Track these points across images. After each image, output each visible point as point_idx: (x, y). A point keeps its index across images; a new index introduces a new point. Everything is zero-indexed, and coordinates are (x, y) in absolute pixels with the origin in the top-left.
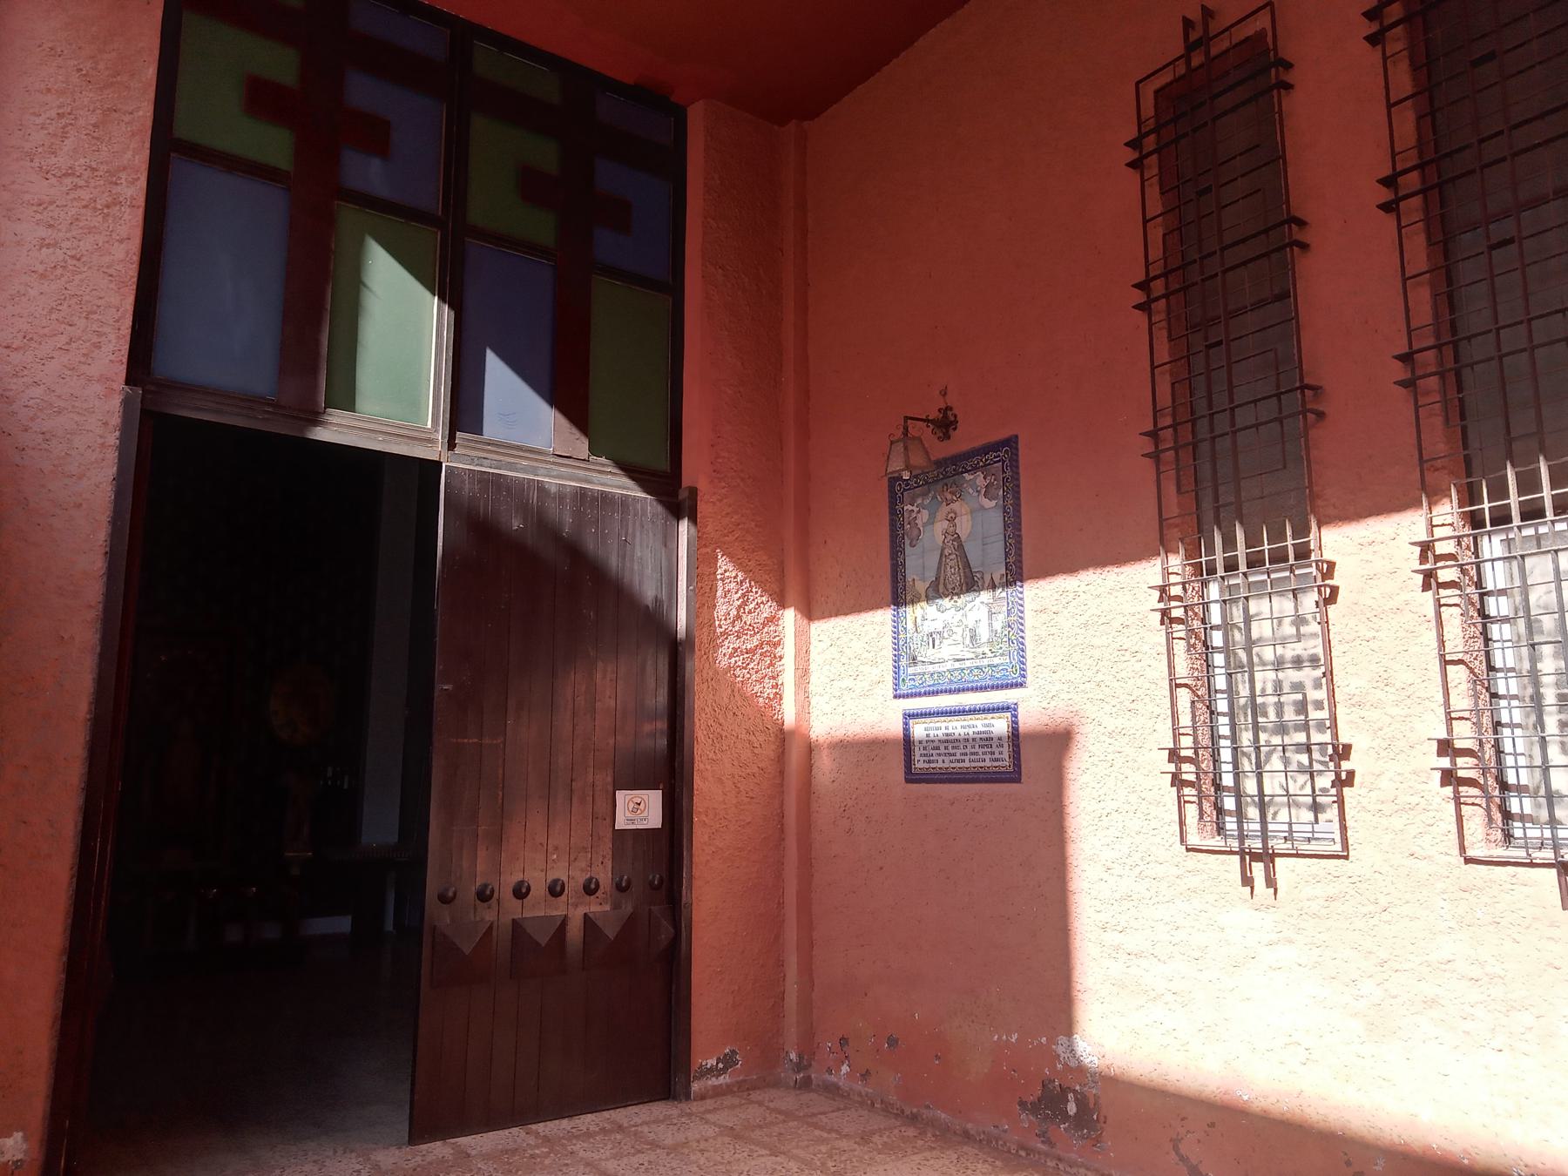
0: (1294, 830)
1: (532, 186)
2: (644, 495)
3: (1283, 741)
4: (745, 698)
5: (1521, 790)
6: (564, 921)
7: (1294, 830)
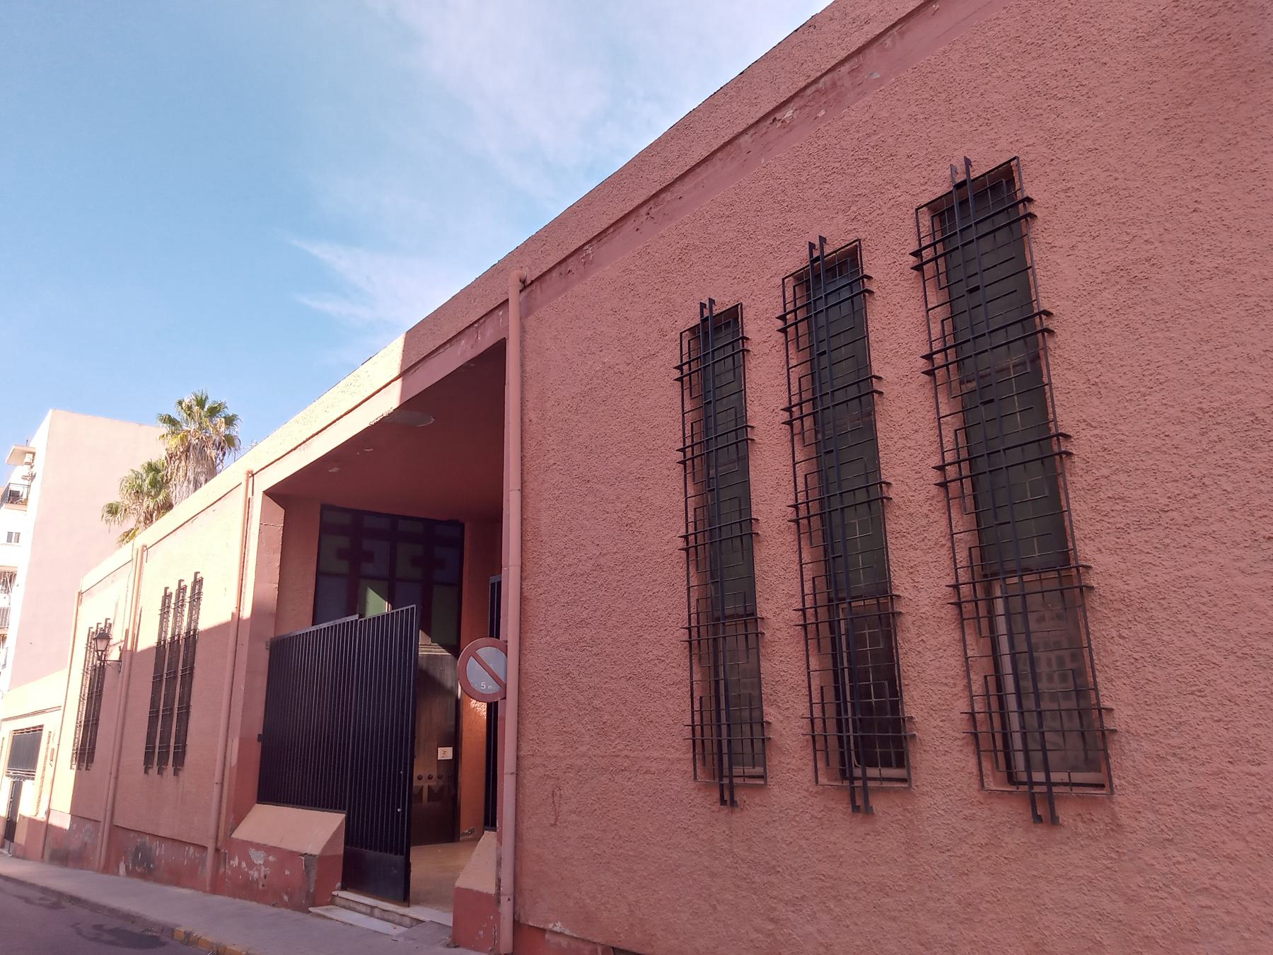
0: (734, 774)
1: (341, 554)
2: (447, 654)
3: (1078, 705)
4: (480, 717)
5: (827, 316)
6: (422, 787)
7: (734, 774)
